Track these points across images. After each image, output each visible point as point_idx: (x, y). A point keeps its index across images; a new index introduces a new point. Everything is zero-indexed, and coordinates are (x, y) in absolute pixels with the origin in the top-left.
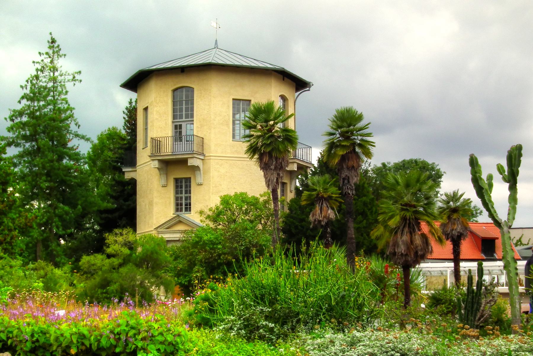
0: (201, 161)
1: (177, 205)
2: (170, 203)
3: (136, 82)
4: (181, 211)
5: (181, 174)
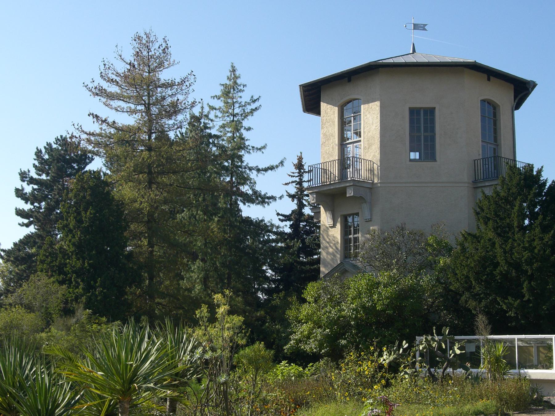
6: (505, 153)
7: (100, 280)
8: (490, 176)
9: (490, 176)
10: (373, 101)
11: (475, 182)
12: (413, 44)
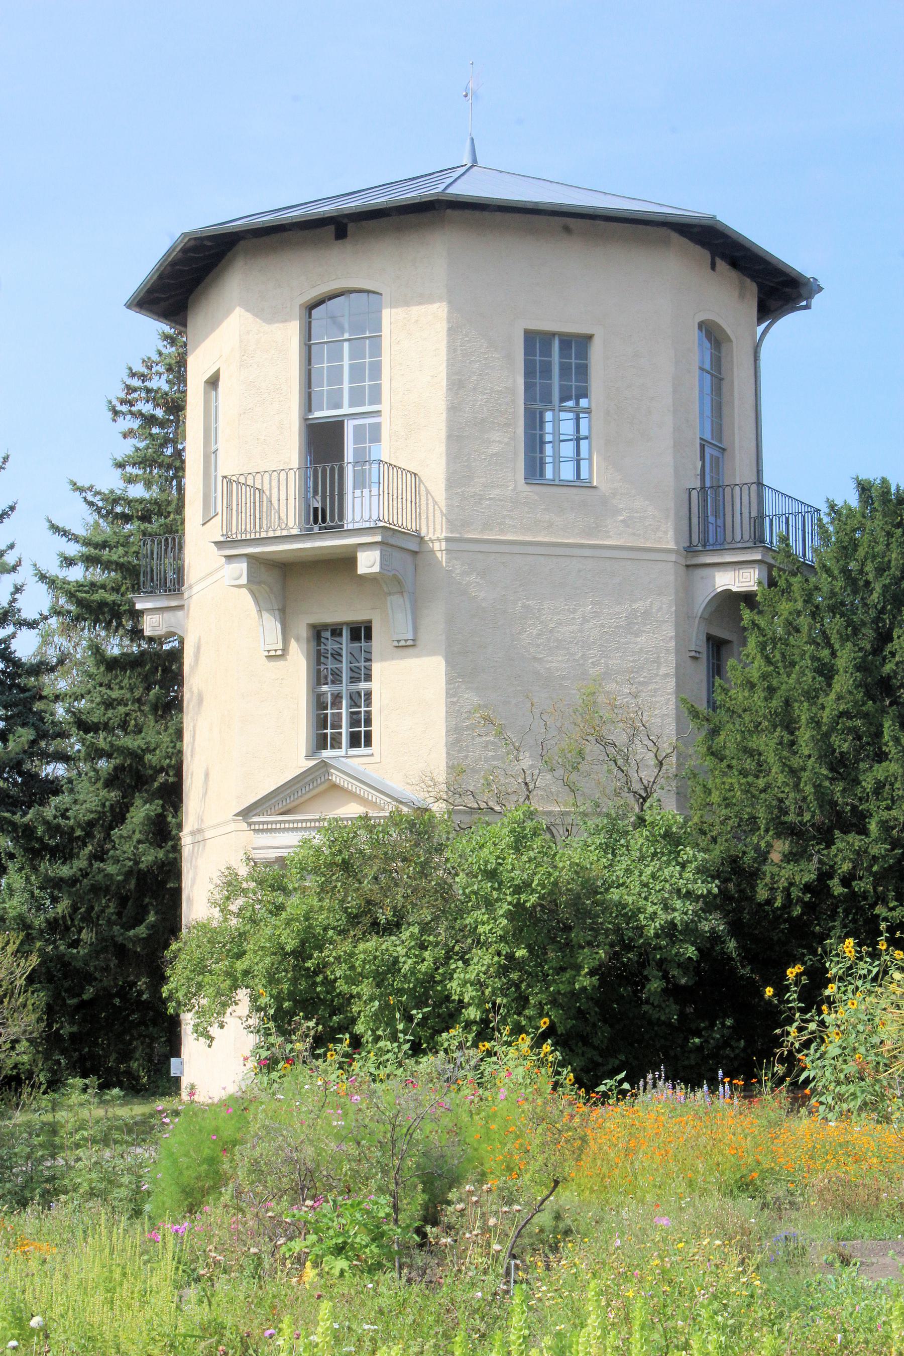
0: (408, 558)
1: (322, 722)
2: (198, 648)
3: (182, 285)
4: (336, 743)
5: (341, 610)
6: (739, 470)
7: (350, 1352)
8: (738, 538)
9: (738, 538)
10: (424, 299)
11: (690, 550)
12: (472, 139)
